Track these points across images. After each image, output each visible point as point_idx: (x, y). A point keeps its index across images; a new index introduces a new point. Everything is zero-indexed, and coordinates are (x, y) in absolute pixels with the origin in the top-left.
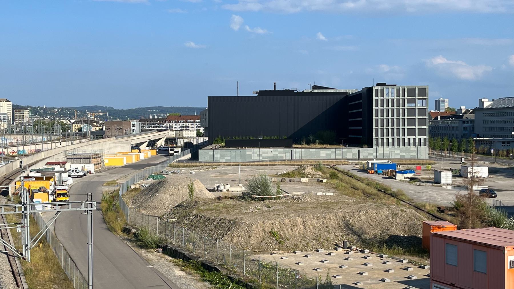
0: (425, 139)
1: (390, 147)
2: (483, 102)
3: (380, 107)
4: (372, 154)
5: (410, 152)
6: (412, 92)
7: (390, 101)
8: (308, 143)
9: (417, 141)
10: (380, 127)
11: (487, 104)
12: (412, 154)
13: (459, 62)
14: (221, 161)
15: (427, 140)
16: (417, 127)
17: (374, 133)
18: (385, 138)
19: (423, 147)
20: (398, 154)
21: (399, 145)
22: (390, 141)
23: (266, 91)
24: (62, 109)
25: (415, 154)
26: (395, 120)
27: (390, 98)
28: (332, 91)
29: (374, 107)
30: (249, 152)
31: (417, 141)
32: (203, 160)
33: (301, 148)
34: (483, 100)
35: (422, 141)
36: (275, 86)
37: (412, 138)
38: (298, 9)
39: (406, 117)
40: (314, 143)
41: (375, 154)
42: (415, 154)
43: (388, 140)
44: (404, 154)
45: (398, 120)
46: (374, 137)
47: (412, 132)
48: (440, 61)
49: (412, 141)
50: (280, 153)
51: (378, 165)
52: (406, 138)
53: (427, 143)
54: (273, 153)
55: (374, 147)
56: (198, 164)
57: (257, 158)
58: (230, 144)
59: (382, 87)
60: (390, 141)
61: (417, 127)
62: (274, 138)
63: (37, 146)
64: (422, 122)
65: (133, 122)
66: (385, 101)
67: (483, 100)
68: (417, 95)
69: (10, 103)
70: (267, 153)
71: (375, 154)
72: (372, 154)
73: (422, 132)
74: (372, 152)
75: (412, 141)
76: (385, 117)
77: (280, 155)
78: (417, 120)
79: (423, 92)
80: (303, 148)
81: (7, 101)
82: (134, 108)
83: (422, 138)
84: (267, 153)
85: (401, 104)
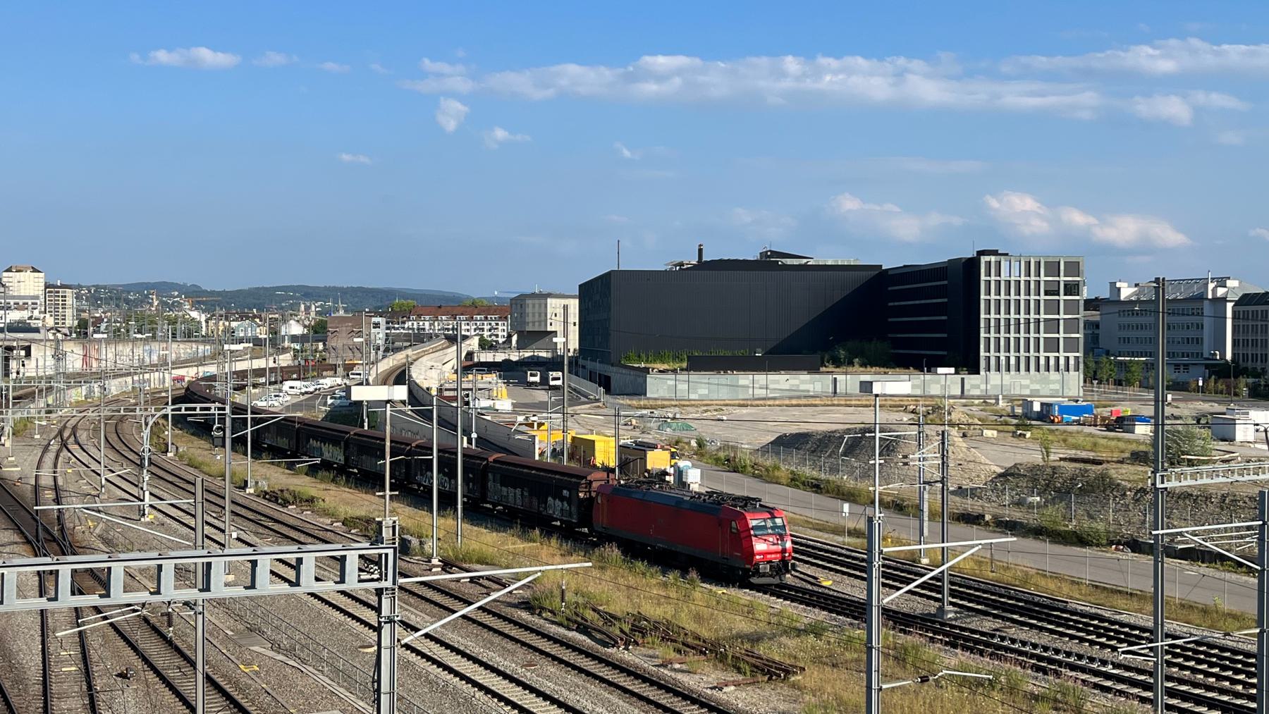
0: (1076, 358)
1: (1013, 372)
2: (1119, 289)
3: (993, 297)
4: (978, 387)
5: (1048, 382)
6: (1053, 268)
7: (1013, 284)
8: (837, 363)
9: (1062, 361)
10: (993, 335)
11: (1126, 292)
12: (1052, 386)
13: (889, 207)
14: (692, 396)
15: (1081, 360)
16: (1062, 335)
17: (982, 346)
18: (1013, 355)
19: (1072, 372)
20: (1027, 387)
21: (1028, 370)
22: (1013, 361)
23: (721, 260)
24: (97, 287)
25: (1057, 386)
26: (1012, 322)
27: (1013, 278)
28: (795, 262)
29: (983, 297)
30: (744, 379)
31: (1062, 361)
32: (656, 396)
33: (846, 373)
34: (1118, 285)
35: (1072, 362)
36: (700, 251)
37: (1052, 355)
38: (550, 92)
39: (1043, 316)
40: (851, 363)
41: (983, 387)
42: (1057, 386)
43: (1008, 358)
44: (1037, 387)
45: (1028, 322)
46: (982, 353)
47: (1053, 345)
48: (849, 204)
49: (1052, 362)
50: (803, 382)
51: (1060, 407)
52: (1042, 355)
53: (1081, 366)
54: (791, 382)
55: (982, 372)
56: (646, 402)
57: (761, 393)
58: (698, 364)
59: (998, 258)
60: (1013, 361)
61: (1062, 335)
62: (739, 353)
63: (491, 360)
64: (1071, 326)
65: (375, 320)
66: (1003, 284)
67: (1118, 285)
68: (1062, 273)
69: (42, 275)
70: (778, 382)
71: (983, 387)
72: (978, 387)
73: (1071, 345)
74: (977, 382)
75: (1052, 362)
76: (1003, 316)
77: (802, 387)
78: (1062, 322)
79: (1073, 268)
80: (851, 374)
81: (35, 270)
82: (246, 288)
83: (1072, 355)
84: (778, 382)
85: (1032, 291)
